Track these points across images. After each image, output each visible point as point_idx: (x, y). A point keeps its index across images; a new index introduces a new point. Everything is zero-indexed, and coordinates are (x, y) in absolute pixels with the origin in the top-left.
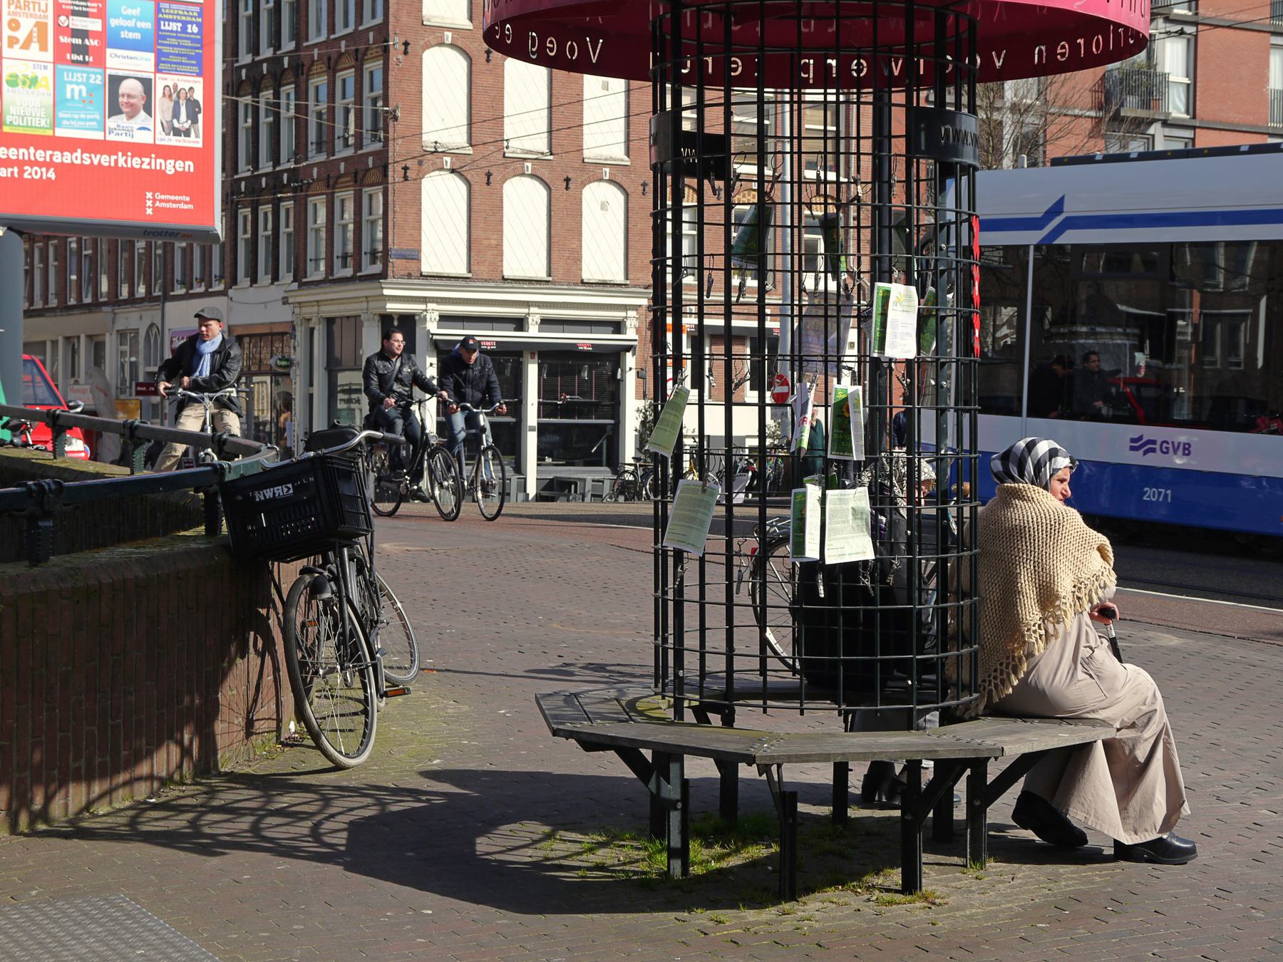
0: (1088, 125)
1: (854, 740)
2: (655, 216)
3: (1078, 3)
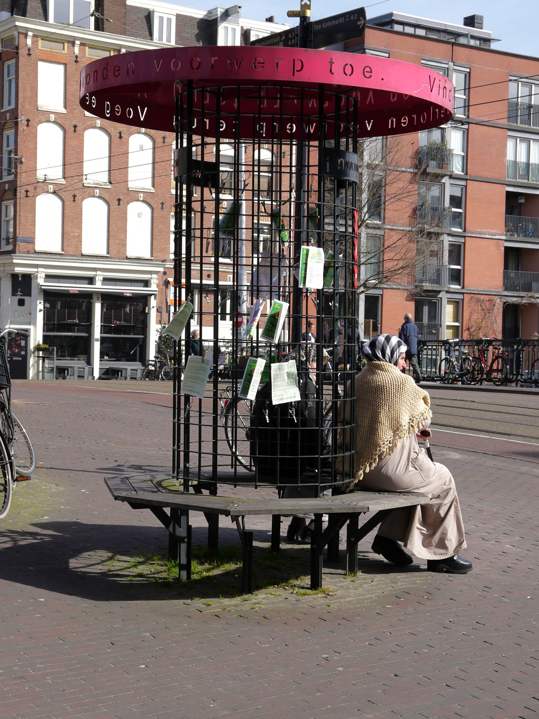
0: (409, 176)
1: (286, 503)
2: (176, 206)
3: (415, 92)
